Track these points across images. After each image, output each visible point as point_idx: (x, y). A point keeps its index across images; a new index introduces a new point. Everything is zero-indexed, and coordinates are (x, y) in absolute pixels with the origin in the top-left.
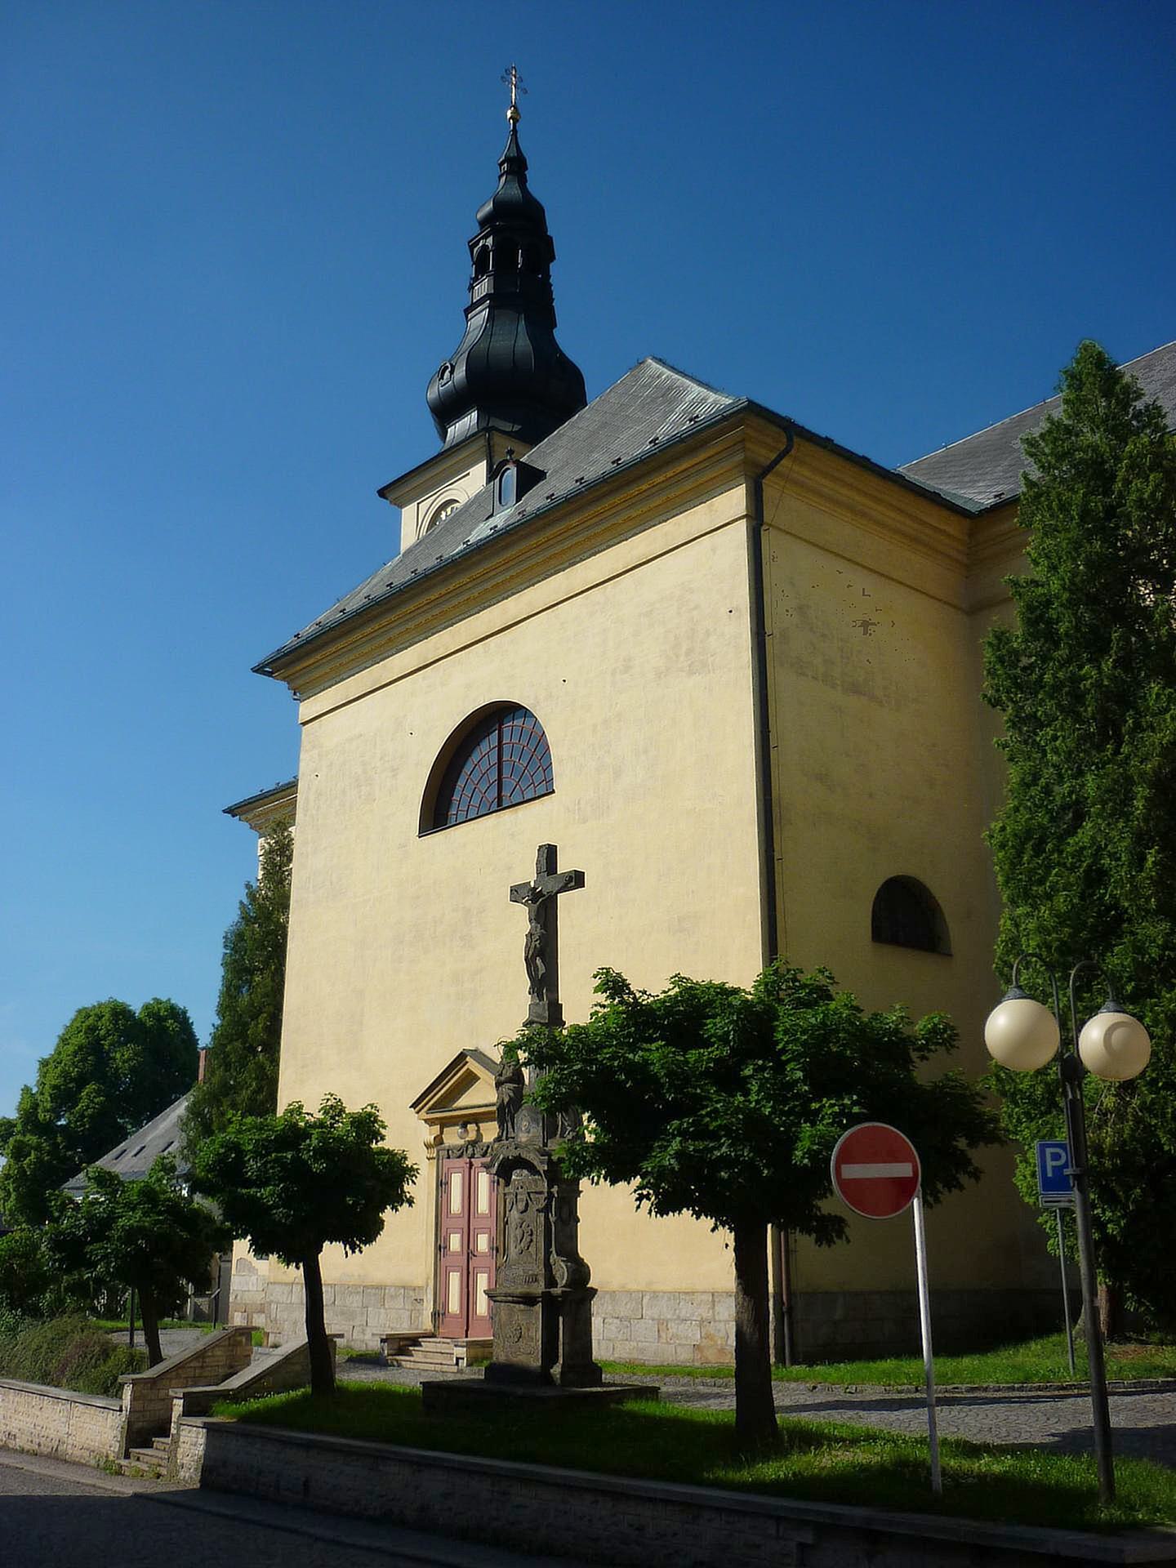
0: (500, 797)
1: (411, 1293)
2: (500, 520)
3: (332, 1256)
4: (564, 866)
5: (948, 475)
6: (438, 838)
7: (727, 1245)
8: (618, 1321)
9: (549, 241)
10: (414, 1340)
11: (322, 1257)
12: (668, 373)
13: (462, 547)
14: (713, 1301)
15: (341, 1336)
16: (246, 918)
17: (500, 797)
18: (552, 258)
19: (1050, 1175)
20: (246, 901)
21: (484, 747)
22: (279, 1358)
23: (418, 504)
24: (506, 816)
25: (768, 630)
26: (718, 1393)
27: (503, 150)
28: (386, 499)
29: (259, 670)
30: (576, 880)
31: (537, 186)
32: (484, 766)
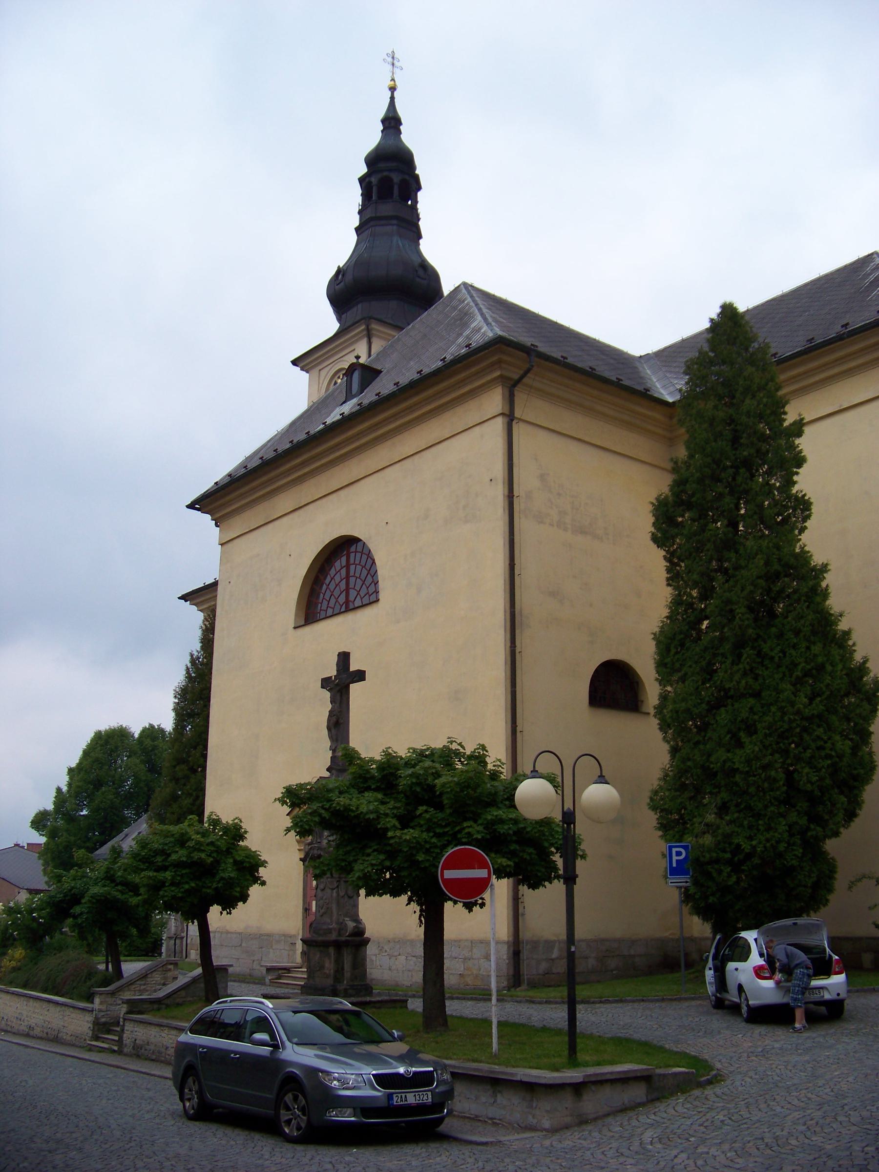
0: (347, 602)
1: (289, 939)
2: (347, 408)
3: (215, 914)
4: (353, 667)
5: (675, 365)
6: (308, 629)
7: (415, 912)
8: (414, 959)
9: (416, 178)
10: (288, 970)
11: (209, 916)
12: (469, 299)
13: (322, 426)
14: (472, 946)
15: (231, 966)
16: (189, 677)
17: (347, 602)
18: (419, 188)
19: (674, 865)
20: (189, 665)
21: (337, 564)
22: (190, 979)
23: (320, 370)
24: (350, 617)
25: (516, 493)
26: (90, 979)
27: (382, 112)
28: (297, 366)
29: (191, 506)
30: (360, 676)
31: (409, 137)
32: (338, 579)
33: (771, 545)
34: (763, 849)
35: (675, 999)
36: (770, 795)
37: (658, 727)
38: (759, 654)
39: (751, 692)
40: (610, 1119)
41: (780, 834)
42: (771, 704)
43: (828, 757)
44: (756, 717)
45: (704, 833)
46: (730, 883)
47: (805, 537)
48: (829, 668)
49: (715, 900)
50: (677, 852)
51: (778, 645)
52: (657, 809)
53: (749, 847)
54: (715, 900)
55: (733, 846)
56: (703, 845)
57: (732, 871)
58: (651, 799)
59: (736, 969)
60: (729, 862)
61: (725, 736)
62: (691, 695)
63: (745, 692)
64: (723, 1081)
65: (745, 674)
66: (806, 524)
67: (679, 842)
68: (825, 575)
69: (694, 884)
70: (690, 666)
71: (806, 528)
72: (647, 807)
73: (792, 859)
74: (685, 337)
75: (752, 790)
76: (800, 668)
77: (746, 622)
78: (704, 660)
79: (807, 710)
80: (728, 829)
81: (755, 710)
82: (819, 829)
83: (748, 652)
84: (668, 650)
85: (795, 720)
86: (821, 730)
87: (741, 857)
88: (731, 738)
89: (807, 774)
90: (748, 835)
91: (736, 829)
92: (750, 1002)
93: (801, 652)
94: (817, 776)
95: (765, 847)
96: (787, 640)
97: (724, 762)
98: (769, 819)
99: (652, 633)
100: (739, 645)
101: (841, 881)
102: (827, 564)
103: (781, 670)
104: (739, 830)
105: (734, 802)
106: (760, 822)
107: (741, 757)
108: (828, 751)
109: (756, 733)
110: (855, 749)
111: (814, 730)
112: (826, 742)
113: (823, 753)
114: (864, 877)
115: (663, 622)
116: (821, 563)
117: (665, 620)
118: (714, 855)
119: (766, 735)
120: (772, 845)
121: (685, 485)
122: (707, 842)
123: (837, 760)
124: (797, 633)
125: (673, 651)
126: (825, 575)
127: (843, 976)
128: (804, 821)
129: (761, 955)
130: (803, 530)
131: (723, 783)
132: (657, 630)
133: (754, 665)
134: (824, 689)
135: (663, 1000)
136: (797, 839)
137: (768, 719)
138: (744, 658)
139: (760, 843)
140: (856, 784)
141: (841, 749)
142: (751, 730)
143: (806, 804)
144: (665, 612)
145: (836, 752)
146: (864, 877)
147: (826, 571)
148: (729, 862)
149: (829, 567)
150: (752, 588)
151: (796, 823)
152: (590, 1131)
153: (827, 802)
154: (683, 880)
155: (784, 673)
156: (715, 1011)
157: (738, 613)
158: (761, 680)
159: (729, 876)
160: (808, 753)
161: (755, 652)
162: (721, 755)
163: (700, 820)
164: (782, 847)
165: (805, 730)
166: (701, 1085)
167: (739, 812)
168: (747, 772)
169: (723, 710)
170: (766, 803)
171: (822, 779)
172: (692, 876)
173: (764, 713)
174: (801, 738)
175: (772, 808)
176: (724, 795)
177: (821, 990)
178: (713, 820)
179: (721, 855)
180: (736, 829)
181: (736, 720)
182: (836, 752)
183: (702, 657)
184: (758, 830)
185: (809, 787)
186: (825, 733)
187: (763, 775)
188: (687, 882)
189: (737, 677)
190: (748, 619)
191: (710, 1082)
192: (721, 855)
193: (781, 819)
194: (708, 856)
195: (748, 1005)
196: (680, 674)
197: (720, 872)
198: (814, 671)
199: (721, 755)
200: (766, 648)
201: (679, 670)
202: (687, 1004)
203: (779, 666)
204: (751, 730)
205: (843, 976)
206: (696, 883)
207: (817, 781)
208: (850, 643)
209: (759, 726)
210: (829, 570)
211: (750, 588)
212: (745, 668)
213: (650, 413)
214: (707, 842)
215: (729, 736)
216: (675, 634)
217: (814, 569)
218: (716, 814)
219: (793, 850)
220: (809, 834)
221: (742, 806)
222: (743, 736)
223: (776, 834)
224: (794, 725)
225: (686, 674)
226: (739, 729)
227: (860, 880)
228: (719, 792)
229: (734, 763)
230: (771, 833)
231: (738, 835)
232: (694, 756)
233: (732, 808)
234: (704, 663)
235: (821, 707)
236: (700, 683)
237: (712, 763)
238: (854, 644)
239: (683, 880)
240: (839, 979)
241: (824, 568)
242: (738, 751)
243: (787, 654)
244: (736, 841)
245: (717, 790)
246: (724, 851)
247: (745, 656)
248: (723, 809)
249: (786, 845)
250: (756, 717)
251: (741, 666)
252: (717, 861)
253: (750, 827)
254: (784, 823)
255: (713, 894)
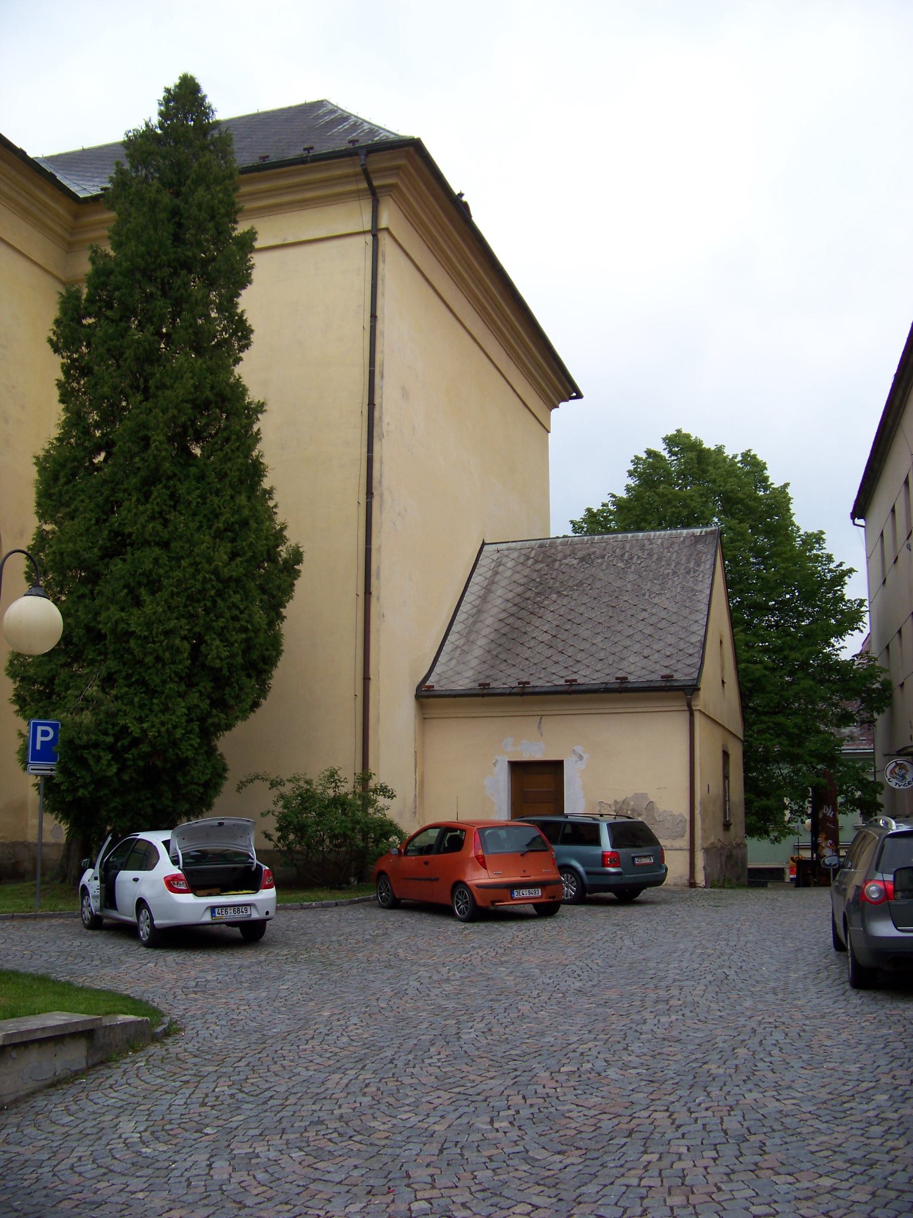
19: (38, 747)
33: (204, 366)
34: (156, 734)
35: (29, 917)
36: (170, 668)
37: (25, 576)
38: (172, 496)
39: (157, 539)
40: (40, 1102)
41: (178, 717)
42: (182, 557)
43: (245, 630)
44: (161, 571)
45: (82, 710)
46: (109, 774)
47: (238, 370)
48: (254, 525)
49: (86, 793)
50: (43, 731)
51: (198, 488)
52: (18, 676)
53: (138, 731)
54: (86, 793)
55: (117, 729)
56: (81, 723)
57: (113, 759)
58: (11, 663)
59: (136, 880)
60: (111, 748)
61: (121, 591)
62: (81, 535)
63: (151, 539)
64: (180, 1030)
65: (152, 518)
66: (241, 355)
67: (46, 719)
68: (260, 416)
69: (61, 772)
70: (82, 501)
71: (241, 359)
72: (4, 673)
73: (187, 750)
74: (86, 147)
75: (149, 659)
76: (223, 519)
77: (164, 454)
78: (101, 495)
79: (226, 570)
80: (113, 707)
81: (160, 561)
82: (222, 716)
83: (158, 492)
84: (56, 478)
85: (210, 580)
86: (238, 597)
87: (126, 742)
88: (127, 594)
89: (217, 647)
90: (138, 716)
91: (124, 708)
92: (156, 922)
93: (225, 501)
94: (228, 651)
95: (159, 732)
96: (209, 484)
97: (117, 622)
98: (166, 698)
99: (35, 457)
100: (150, 481)
101: (228, 787)
102: (263, 404)
103: (198, 518)
104: (128, 708)
105: (124, 673)
106: (155, 701)
107: (139, 618)
108: (243, 623)
109: (160, 590)
110: (271, 624)
111: (230, 596)
112: (242, 612)
113: (238, 625)
114: (257, 777)
115: (52, 443)
116: (256, 401)
117: (55, 442)
118: (93, 737)
119: (172, 594)
120: (167, 730)
121: (108, 277)
122: (86, 721)
123: (252, 634)
124: (222, 476)
125: (62, 480)
126: (260, 416)
127: (274, 889)
128: (205, 705)
129: (175, 862)
130: (238, 360)
131: (112, 648)
132: (41, 453)
133: (164, 508)
134: (246, 548)
135: (13, 918)
136: (195, 726)
137: (178, 574)
138: (153, 497)
139: (153, 726)
140: (266, 667)
141: (259, 623)
142: (154, 586)
143: (211, 684)
144: (56, 432)
145: (252, 625)
146: (257, 777)
147: (262, 412)
148: (111, 748)
149: (265, 408)
150: (176, 412)
151: (197, 706)
152: (18, 1126)
153: (235, 685)
154: (48, 768)
155: (201, 522)
156: (90, 932)
157: (155, 441)
158: (171, 528)
159: (109, 765)
160: (221, 623)
161: (168, 493)
162: (114, 613)
163: (77, 693)
164: (179, 733)
165: (220, 594)
166: (156, 1039)
167: (129, 686)
168: (146, 637)
169: (117, 560)
170: (164, 677)
171: (233, 656)
172: (60, 763)
173: (172, 569)
174: (214, 602)
175: (172, 685)
176: (112, 664)
177: (248, 908)
178: (95, 693)
179: (102, 738)
180: (124, 708)
181: (136, 572)
182: (252, 625)
183: (97, 492)
184: (151, 710)
185: (217, 664)
186: (242, 600)
187: (165, 643)
188: (52, 770)
189: (142, 519)
190: (166, 450)
191: (167, 1034)
192: (102, 738)
193: (180, 700)
194: (85, 738)
195: (152, 926)
196: (68, 510)
197: (98, 759)
198: (237, 526)
199: (114, 613)
200: (182, 489)
201: (68, 506)
202: (45, 923)
203: (194, 515)
204: (154, 586)
205: (274, 889)
206: (64, 770)
207: (228, 657)
208: (271, 503)
209: (165, 582)
210: (265, 411)
211: (173, 412)
212: (153, 509)
213: (51, 203)
214: (86, 721)
215: (126, 591)
216: (66, 460)
217: (248, 407)
218: (98, 686)
219: (189, 738)
220: (210, 721)
221: (133, 680)
222: (144, 593)
223: (174, 718)
224: (209, 586)
225: (76, 510)
226: (140, 584)
227: (252, 781)
228: (105, 660)
229: (129, 624)
230: (167, 716)
231: (125, 714)
232: (77, 611)
233: (121, 681)
234: (100, 499)
235: (241, 570)
236: (93, 521)
237: (99, 622)
238: (276, 506)
239: (48, 768)
240: (268, 894)
241: (260, 408)
242: (135, 610)
243: (208, 501)
244: (122, 722)
245: (102, 657)
246: (106, 734)
247: (155, 494)
248: (108, 681)
249: (183, 732)
250: (161, 571)
251: (149, 506)
252: (96, 745)
253: (142, 706)
254: (183, 704)
255: (84, 786)
